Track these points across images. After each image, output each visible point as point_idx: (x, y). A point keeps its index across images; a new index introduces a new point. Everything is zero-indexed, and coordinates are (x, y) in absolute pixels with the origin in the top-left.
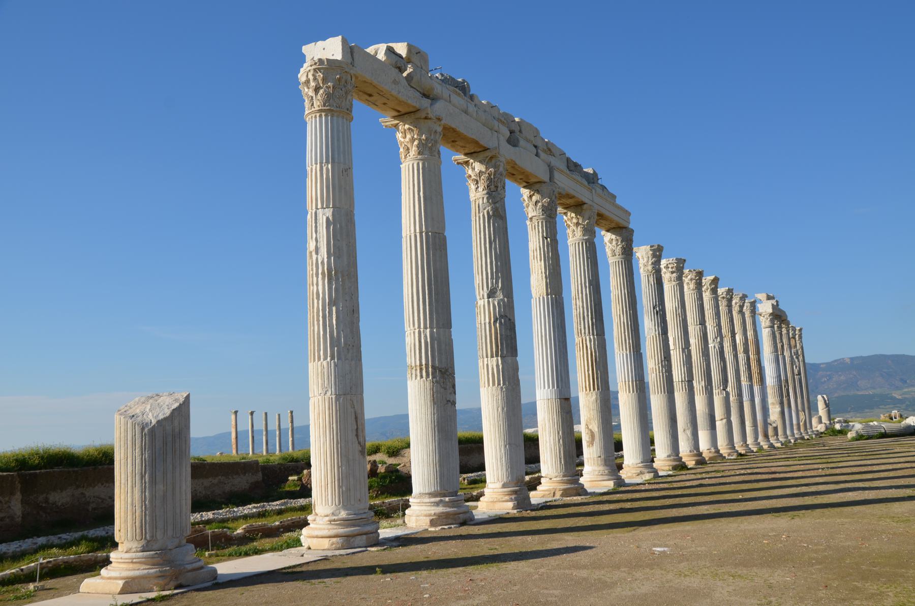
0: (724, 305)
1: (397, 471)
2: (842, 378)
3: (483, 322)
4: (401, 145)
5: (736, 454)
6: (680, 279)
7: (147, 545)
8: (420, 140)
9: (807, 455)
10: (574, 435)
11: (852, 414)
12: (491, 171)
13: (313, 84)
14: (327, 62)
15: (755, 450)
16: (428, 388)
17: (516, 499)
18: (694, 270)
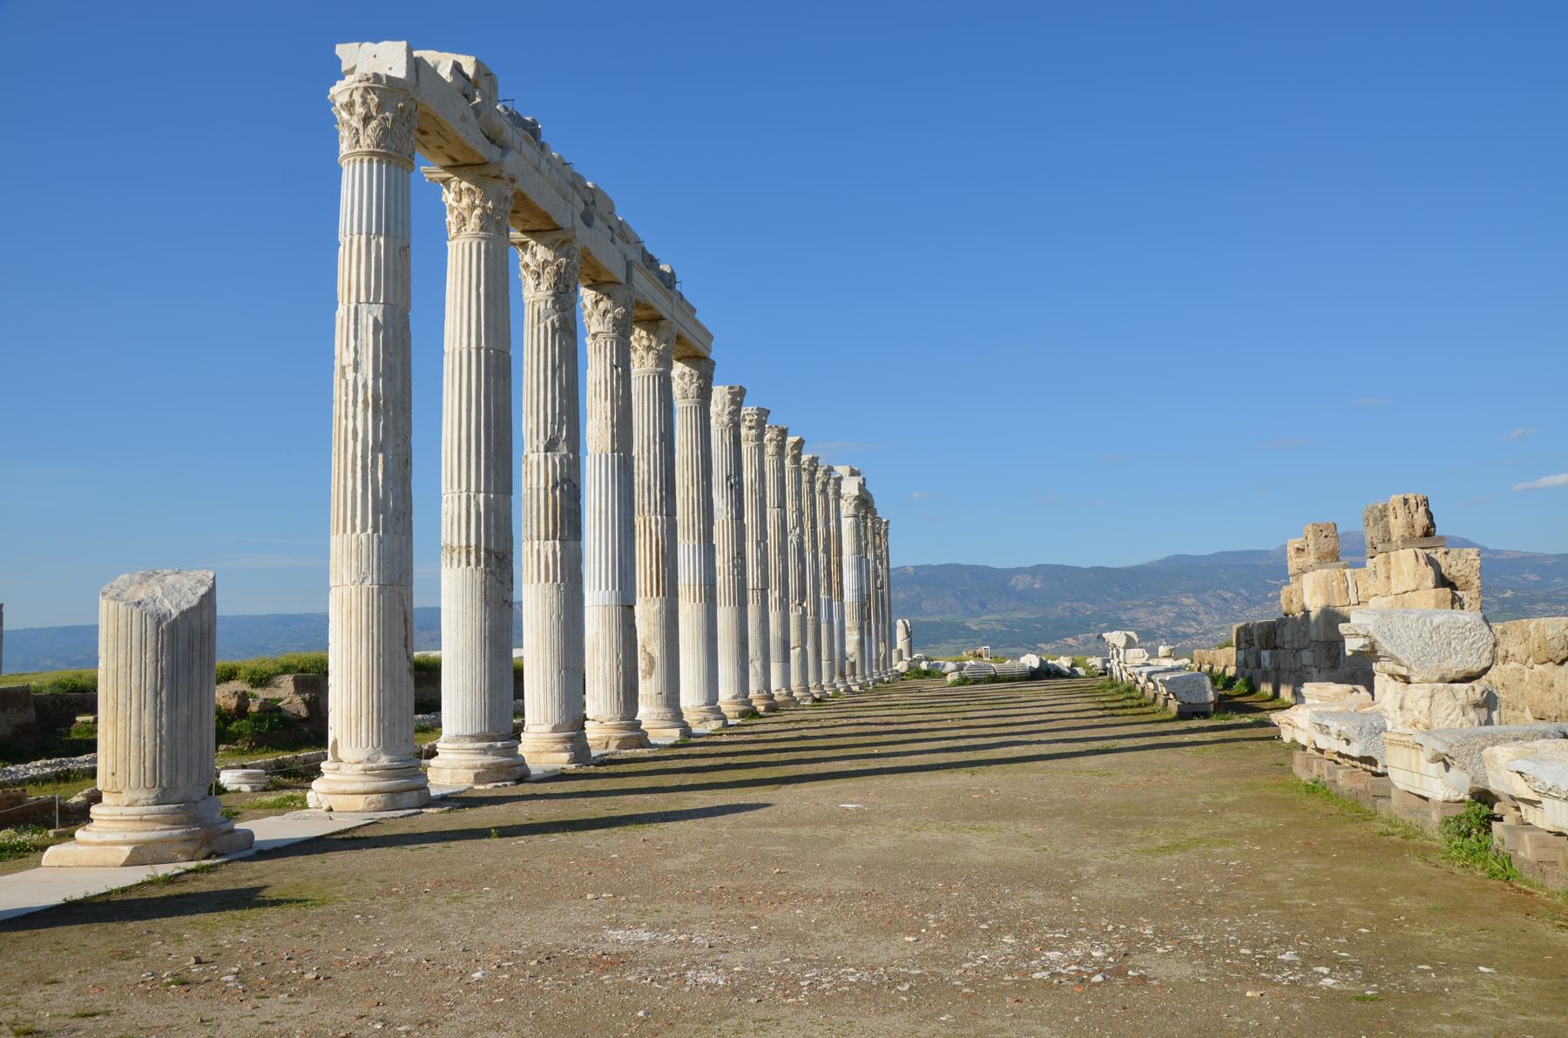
1: (279, 710)
3: (535, 487)
4: (452, 212)
5: (811, 698)
6: (760, 437)
7: (162, 796)
8: (484, 208)
10: (512, 662)
12: (561, 262)
13: (360, 110)
14: (387, 80)
16: (478, 582)
17: (572, 749)
18: (776, 427)
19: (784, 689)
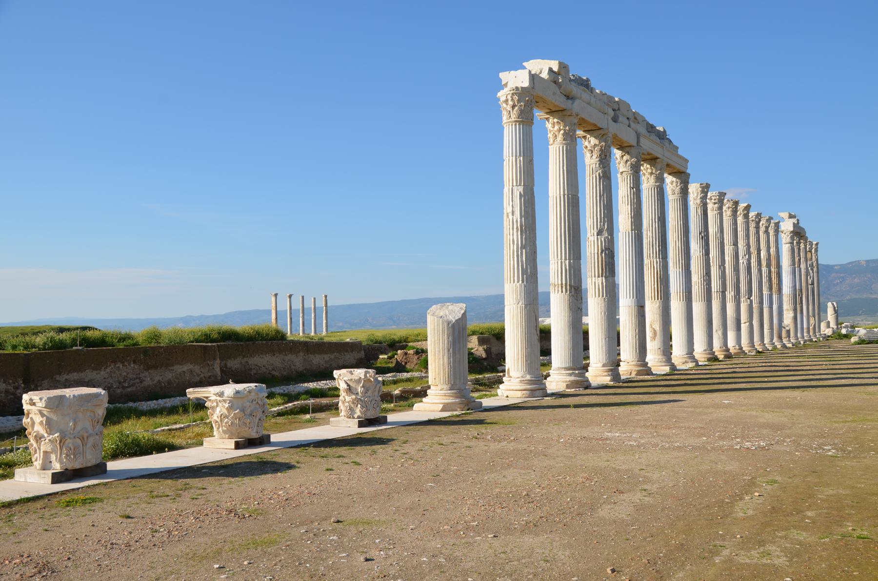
0: (752, 226)
2: (856, 280)
3: (593, 252)
4: (550, 132)
5: (755, 351)
6: (720, 208)
8: (565, 130)
9: (814, 354)
11: (862, 317)
13: (510, 103)
15: (770, 349)
17: (612, 375)
18: (732, 200)
19: (737, 346)
